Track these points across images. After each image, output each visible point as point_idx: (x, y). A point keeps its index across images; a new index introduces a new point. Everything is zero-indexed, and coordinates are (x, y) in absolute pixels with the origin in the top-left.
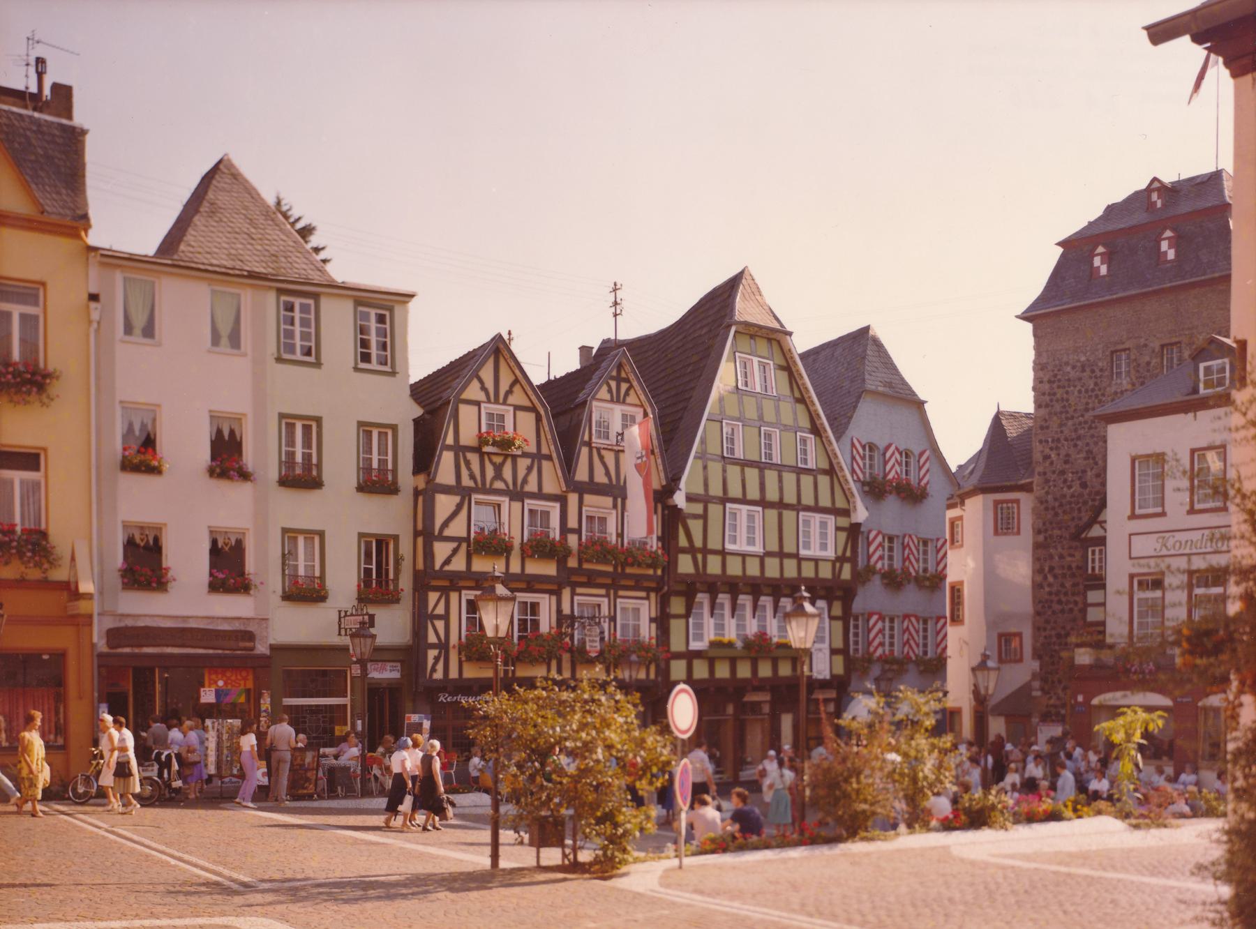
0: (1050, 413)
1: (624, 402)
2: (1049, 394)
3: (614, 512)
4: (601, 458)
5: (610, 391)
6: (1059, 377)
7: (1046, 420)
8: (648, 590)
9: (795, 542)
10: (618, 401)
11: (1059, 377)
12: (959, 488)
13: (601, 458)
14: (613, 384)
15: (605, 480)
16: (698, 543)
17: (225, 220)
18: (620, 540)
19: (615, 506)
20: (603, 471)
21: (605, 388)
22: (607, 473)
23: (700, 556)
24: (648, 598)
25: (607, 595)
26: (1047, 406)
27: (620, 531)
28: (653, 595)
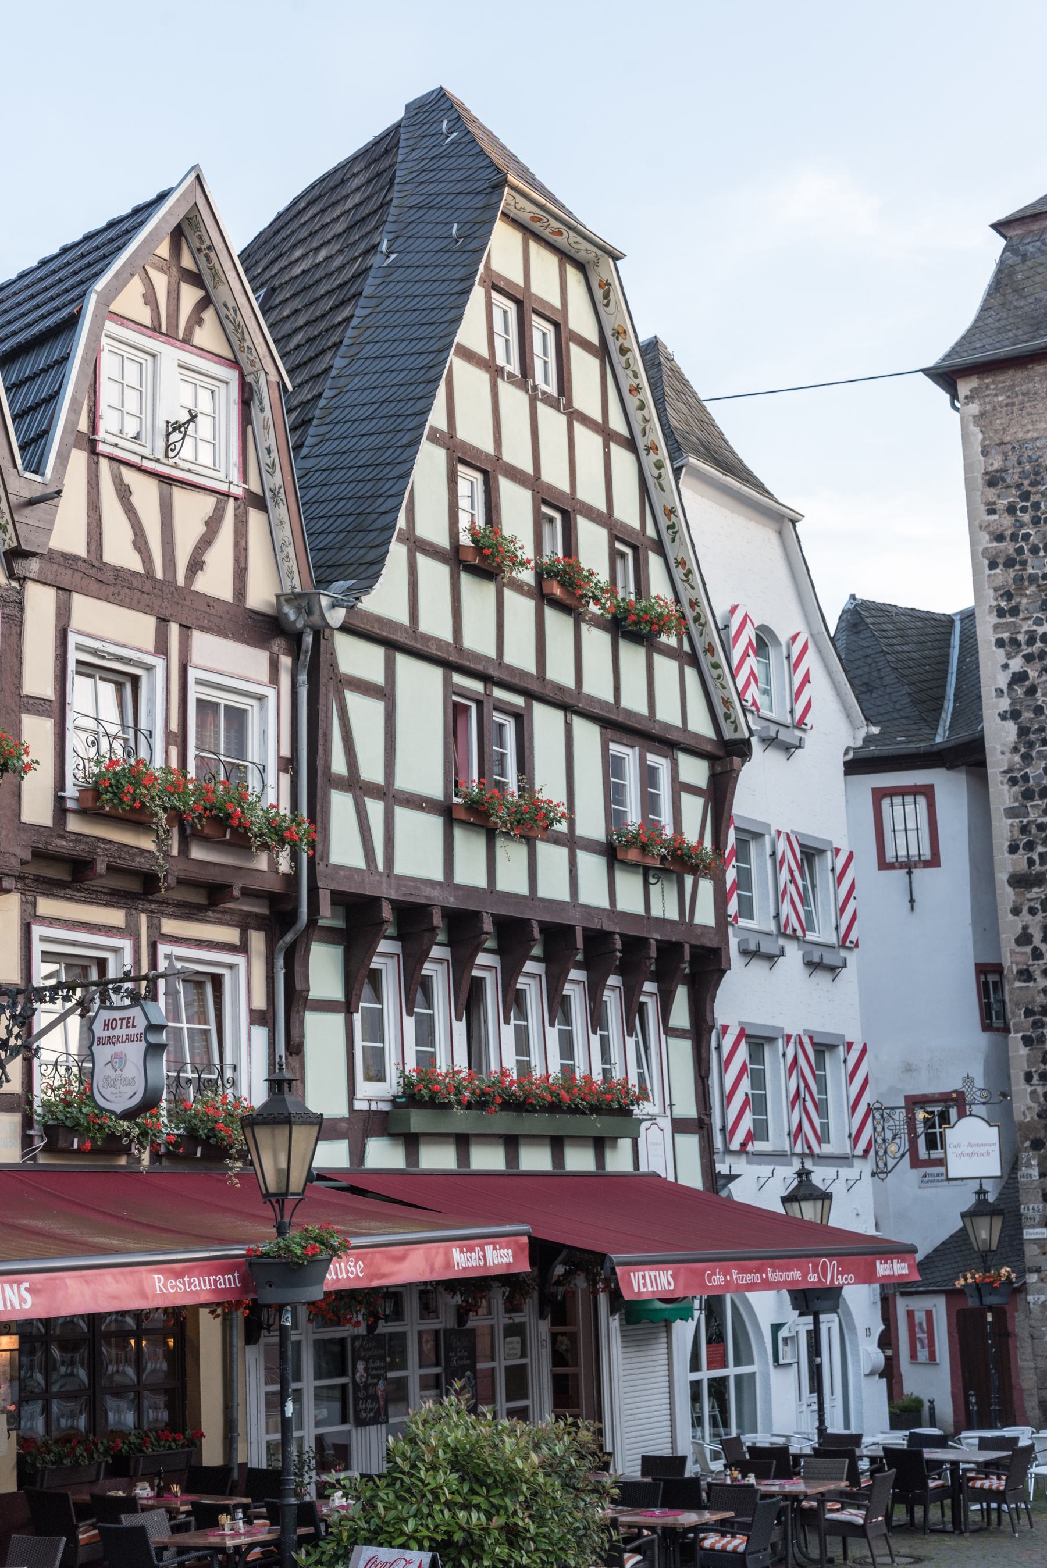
0: (1019, 580)
1: (187, 341)
2: (1014, 537)
3: (159, 662)
4: (124, 493)
5: (150, 298)
6: (1034, 498)
7: (1009, 596)
8: (245, 924)
9: (5, 442)
10: (171, 337)
11: (1034, 498)
12: (736, 730)
13: (124, 493)
14: (160, 281)
15: (133, 563)
16: (372, 771)
17: (964, 1248)
18: (174, 751)
19: (161, 648)
20: (128, 534)
21: (135, 287)
22: (140, 544)
23: (375, 808)
24: (242, 948)
25: (130, 931)
26: (1009, 563)
27: (174, 727)
28: (257, 940)
